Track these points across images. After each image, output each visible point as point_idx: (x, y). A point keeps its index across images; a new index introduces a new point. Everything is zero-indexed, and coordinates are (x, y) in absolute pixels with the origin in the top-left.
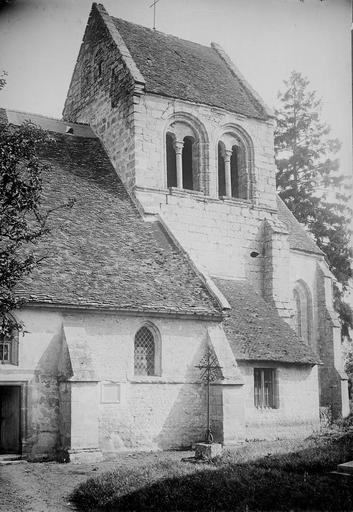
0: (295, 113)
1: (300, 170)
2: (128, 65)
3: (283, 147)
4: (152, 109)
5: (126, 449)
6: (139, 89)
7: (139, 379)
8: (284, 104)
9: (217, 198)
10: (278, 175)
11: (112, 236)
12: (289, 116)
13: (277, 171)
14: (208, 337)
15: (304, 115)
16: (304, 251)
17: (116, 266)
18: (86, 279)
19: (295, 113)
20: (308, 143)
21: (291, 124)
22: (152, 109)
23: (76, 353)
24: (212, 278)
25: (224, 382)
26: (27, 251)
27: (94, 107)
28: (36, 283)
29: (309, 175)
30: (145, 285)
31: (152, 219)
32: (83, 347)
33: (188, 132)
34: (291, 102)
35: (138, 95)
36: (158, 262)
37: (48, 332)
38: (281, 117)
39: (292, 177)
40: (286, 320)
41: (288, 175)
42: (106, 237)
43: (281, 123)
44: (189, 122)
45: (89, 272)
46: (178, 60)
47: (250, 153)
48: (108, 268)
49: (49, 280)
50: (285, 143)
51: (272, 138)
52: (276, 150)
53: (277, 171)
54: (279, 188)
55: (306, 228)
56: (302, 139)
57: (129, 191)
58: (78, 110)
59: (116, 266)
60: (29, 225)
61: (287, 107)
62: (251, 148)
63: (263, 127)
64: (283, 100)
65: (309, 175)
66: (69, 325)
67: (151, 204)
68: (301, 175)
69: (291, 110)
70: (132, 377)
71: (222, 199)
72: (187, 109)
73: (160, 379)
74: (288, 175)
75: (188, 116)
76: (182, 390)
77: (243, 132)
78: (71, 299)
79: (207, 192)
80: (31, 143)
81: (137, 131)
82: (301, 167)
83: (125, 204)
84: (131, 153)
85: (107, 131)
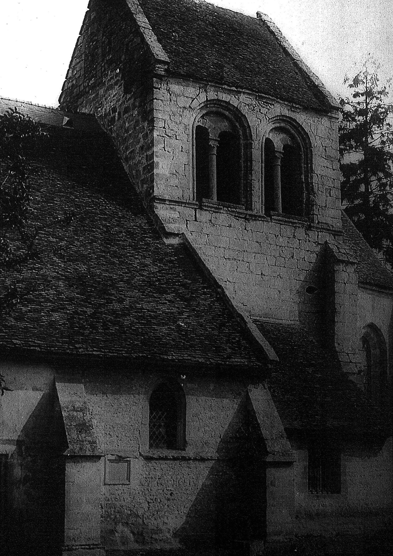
0: (367, 104)
1: (373, 178)
2: (147, 38)
3: (351, 147)
4: (177, 96)
5: (137, 546)
6: (161, 70)
7: (157, 453)
8: (353, 91)
9: (262, 213)
10: (343, 184)
11: (121, 263)
12: (359, 107)
13: (342, 179)
14: (248, 398)
15: (379, 106)
16: (376, 285)
17: (127, 303)
18: (87, 321)
19: (367, 104)
20: (383, 143)
21: (361, 118)
22: (177, 96)
23: (72, 418)
24: (255, 321)
25: (269, 459)
26: (8, 282)
27: (101, 92)
28: (22, 325)
29: (385, 185)
30: (164, 329)
31: (175, 241)
32: (81, 410)
33: (224, 126)
34: (361, 88)
35: (160, 77)
36: (183, 299)
37: (35, 389)
38: (348, 108)
39: (362, 188)
40: (351, 378)
41: (358, 183)
42: (113, 263)
43: (348, 116)
44: (227, 113)
45: (89, 311)
46: (213, 33)
47: (306, 155)
48: (117, 306)
49: (38, 320)
50: (353, 143)
51: (336, 136)
52: (341, 152)
53: (342, 179)
54: (344, 202)
55: (380, 256)
56: (375, 137)
57: (145, 204)
58: (80, 95)
59: (127, 303)
60: (11, 247)
61: (356, 95)
62: (308, 146)
63: (325, 121)
64: (351, 86)
65: (385, 185)
66: (61, 380)
67: (174, 221)
68: (374, 184)
69: (362, 99)
70: (145, 449)
71: (270, 216)
72: (224, 97)
73: (183, 454)
74: (358, 183)
75: (227, 105)
76: (212, 468)
77: (298, 127)
78: (66, 346)
79: (249, 207)
80: (16, 137)
81: (159, 124)
82: (375, 174)
83: (141, 221)
84: (149, 153)
85: (118, 124)
